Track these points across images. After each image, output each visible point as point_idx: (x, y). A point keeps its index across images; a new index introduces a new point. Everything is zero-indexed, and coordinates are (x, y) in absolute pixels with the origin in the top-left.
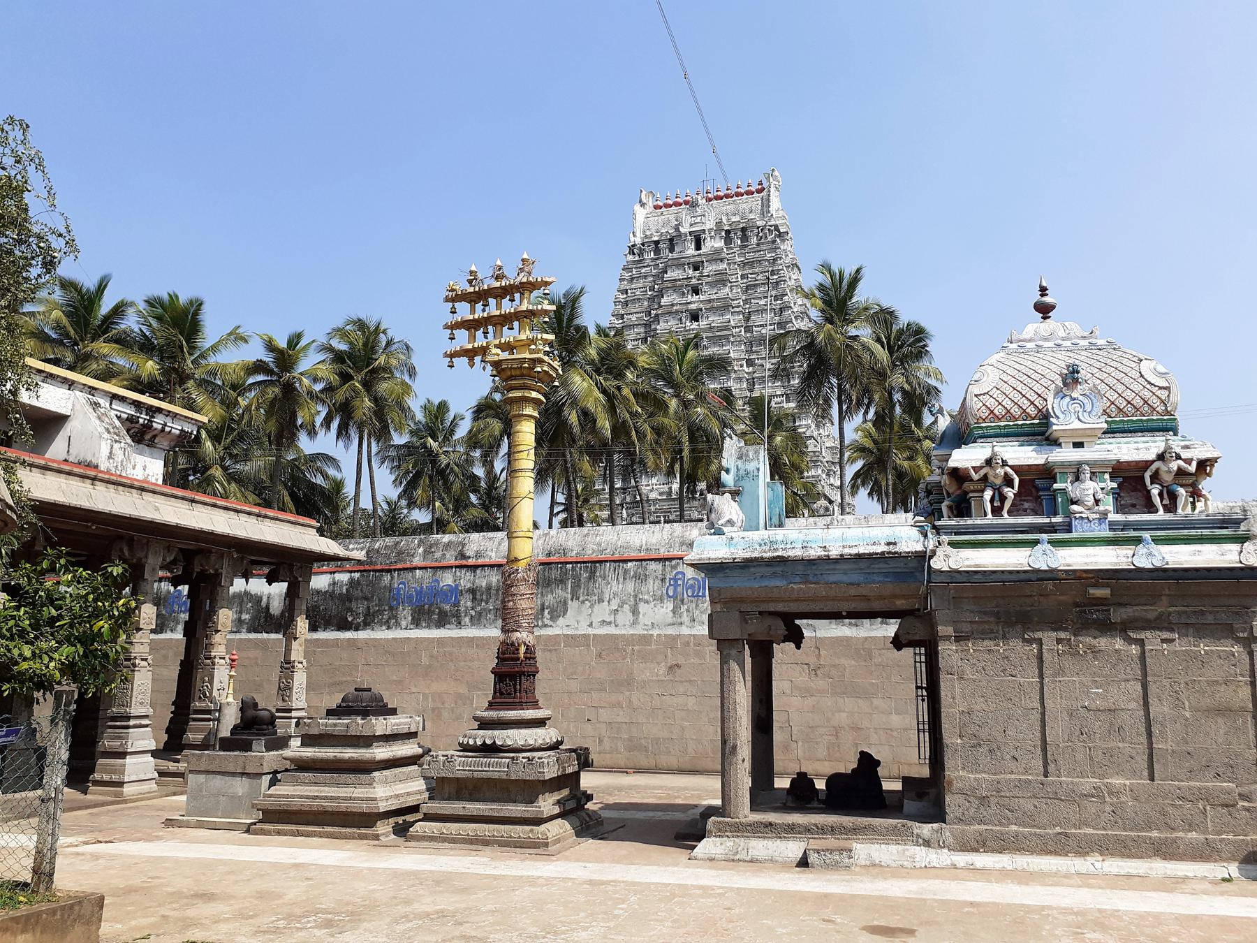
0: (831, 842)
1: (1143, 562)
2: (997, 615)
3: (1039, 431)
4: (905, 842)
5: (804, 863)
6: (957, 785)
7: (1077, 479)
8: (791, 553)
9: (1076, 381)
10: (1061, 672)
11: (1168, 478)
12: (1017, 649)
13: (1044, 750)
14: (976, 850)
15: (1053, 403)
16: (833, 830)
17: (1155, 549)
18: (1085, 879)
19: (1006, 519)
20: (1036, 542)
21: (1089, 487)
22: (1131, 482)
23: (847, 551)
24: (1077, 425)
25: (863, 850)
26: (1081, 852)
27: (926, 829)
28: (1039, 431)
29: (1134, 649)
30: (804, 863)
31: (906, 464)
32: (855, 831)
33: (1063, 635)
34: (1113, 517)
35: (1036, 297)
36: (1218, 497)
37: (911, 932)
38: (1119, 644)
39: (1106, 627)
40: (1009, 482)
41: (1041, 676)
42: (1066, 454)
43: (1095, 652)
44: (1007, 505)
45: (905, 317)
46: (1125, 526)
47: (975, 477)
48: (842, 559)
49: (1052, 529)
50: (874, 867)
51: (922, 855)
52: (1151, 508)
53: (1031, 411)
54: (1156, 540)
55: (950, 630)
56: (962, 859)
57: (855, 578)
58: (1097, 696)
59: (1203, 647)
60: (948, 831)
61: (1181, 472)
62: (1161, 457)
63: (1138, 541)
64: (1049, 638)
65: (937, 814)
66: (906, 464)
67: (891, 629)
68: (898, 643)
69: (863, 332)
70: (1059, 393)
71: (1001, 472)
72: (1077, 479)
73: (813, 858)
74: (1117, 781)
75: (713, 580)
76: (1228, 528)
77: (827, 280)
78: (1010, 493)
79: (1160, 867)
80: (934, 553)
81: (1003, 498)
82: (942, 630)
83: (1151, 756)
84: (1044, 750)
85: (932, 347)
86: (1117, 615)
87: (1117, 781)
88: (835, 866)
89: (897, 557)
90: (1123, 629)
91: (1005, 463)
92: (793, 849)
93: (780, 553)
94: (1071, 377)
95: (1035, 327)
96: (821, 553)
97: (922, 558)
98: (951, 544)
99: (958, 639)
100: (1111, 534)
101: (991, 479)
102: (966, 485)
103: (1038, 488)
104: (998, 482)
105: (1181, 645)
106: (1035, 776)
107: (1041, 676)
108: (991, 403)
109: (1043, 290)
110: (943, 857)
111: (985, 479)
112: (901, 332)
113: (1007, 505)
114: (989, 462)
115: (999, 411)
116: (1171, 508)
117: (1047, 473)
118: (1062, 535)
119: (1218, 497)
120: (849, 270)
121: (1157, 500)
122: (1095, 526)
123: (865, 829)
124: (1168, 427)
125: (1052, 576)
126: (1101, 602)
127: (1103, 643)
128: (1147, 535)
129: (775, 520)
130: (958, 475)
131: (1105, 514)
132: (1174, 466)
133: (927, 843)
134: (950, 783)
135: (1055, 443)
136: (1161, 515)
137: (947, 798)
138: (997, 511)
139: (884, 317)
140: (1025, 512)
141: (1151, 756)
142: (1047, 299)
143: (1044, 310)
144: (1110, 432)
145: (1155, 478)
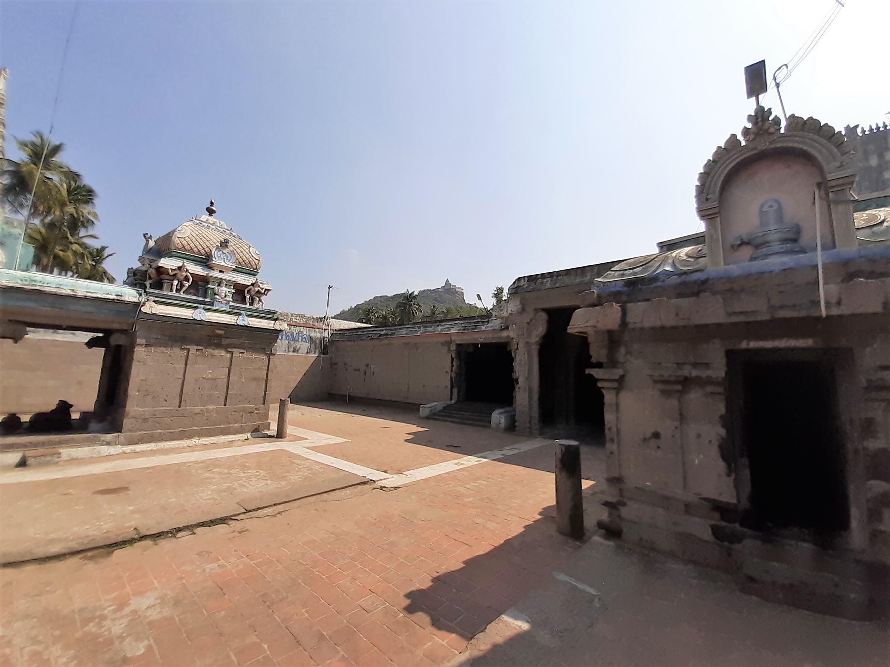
0: (41, 450)
1: (240, 323)
2: (170, 337)
3: (205, 261)
4: (94, 445)
5: (23, 464)
6: (132, 414)
7: (219, 285)
8: (47, 289)
9: (227, 246)
10: (196, 363)
11: (253, 293)
12: (177, 352)
13: (181, 396)
14: (137, 443)
15: (213, 250)
16: (43, 444)
17: (247, 318)
18: (193, 448)
19: (181, 295)
20: (197, 308)
21: (224, 290)
22: (240, 292)
23: (89, 294)
24: (223, 264)
25: (66, 452)
26: (190, 437)
27: (109, 437)
28: (205, 261)
29: (229, 355)
30: (23, 464)
31: (61, 253)
32: (60, 443)
33: (200, 348)
34: (231, 303)
35: (209, 205)
36: (266, 303)
37: (126, 489)
38: (223, 353)
39: (219, 346)
40: (188, 280)
41: (186, 365)
42: (216, 274)
43: (212, 356)
44: (184, 289)
45: (88, 180)
46: (236, 307)
47: (171, 273)
48: (85, 298)
49: (204, 303)
50: (74, 461)
51: (105, 450)
52: (244, 302)
53: (203, 252)
54: (248, 315)
55: (143, 341)
56: (128, 449)
57: (89, 309)
58: (209, 374)
59: (254, 356)
60: (121, 436)
61: (258, 292)
62: (253, 285)
63: (240, 314)
64: (193, 348)
65: (115, 427)
66: (61, 253)
67: (87, 336)
68: (91, 344)
69: (56, 178)
70: (217, 248)
71: (184, 274)
72: (219, 285)
73: (30, 461)
74: (210, 407)
75: (816, 314)
76: (271, 315)
77: (38, 141)
78: (187, 284)
79: (152, 446)
80: (144, 304)
81: (182, 286)
82: (139, 341)
83: (226, 397)
84: (181, 396)
85: (96, 201)
86: (225, 342)
87: (210, 407)
88: (47, 464)
89: (123, 302)
90: (226, 348)
91: (187, 271)
92: (14, 457)
93: (38, 288)
94: (224, 244)
95: (205, 217)
96: (69, 292)
97: (137, 305)
98: (154, 301)
99: (146, 346)
100: (228, 309)
101: (178, 276)
102: (163, 276)
103: (200, 285)
104: (182, 278)
105: (247, 355)
106: (173, 407)
107: (186, 365)
108: (185, 243)
109: (212, 203)
110: (119, 449)
111: (175, 275)
112: (79, 187)
113: (184, 289)
114: (180, 268)
115: (187, 247)
116: (251, 304)
117: (206, 280)
118: (209, 307)
119: (266, 303)
120: (56, 142)
121: (247, 300)
122: (223, 305)
123: (73, 440)
124: (253, 274)
125: (201, 323)
126: (219, 336)
127: (217, 352)
128: (244, 313)
129: (24, 267)
130: (160, 270)
131: (229, 301)
132: (257, 289)
133: (108, 444)
134: (128, 414)
135: (211, 268)
136: (248, 306)
137: (125, 421)
138: (178, 291)
139: (72, 176)
140: (190, 294)
141: (226, 397)
142: (214, 208)
143: (211, 212)
144: (234, 270)
145: (249, 292)
